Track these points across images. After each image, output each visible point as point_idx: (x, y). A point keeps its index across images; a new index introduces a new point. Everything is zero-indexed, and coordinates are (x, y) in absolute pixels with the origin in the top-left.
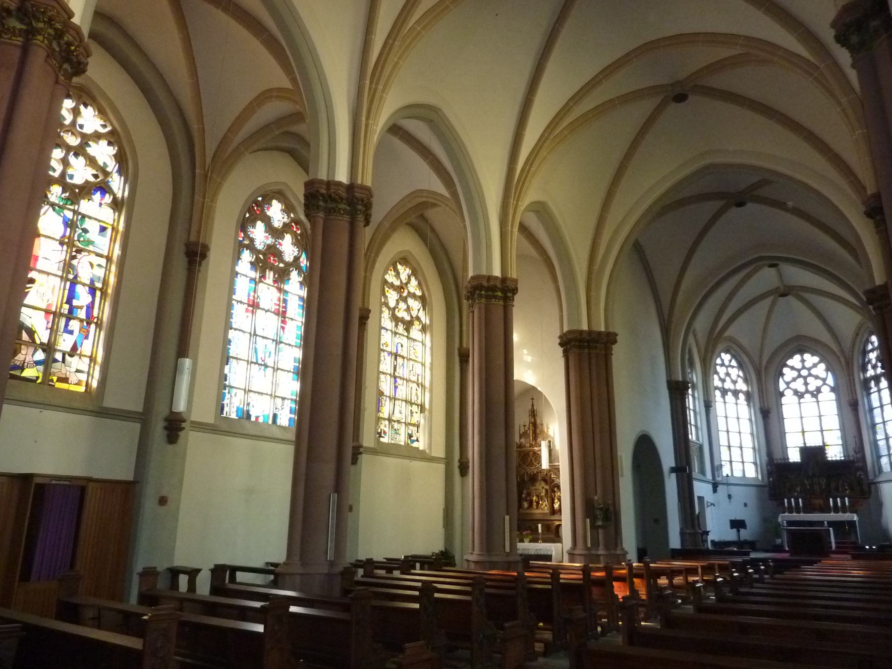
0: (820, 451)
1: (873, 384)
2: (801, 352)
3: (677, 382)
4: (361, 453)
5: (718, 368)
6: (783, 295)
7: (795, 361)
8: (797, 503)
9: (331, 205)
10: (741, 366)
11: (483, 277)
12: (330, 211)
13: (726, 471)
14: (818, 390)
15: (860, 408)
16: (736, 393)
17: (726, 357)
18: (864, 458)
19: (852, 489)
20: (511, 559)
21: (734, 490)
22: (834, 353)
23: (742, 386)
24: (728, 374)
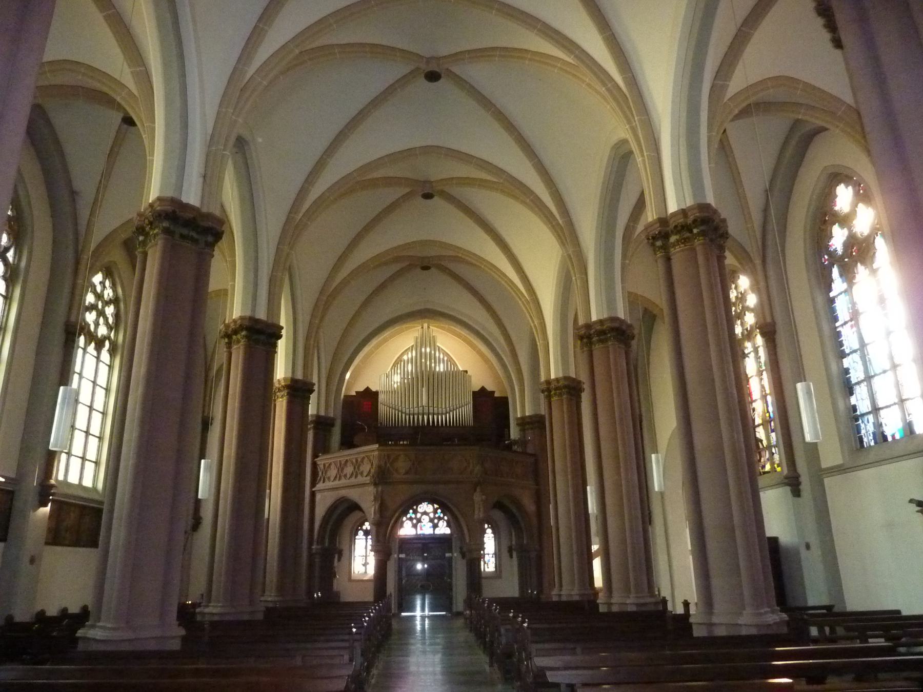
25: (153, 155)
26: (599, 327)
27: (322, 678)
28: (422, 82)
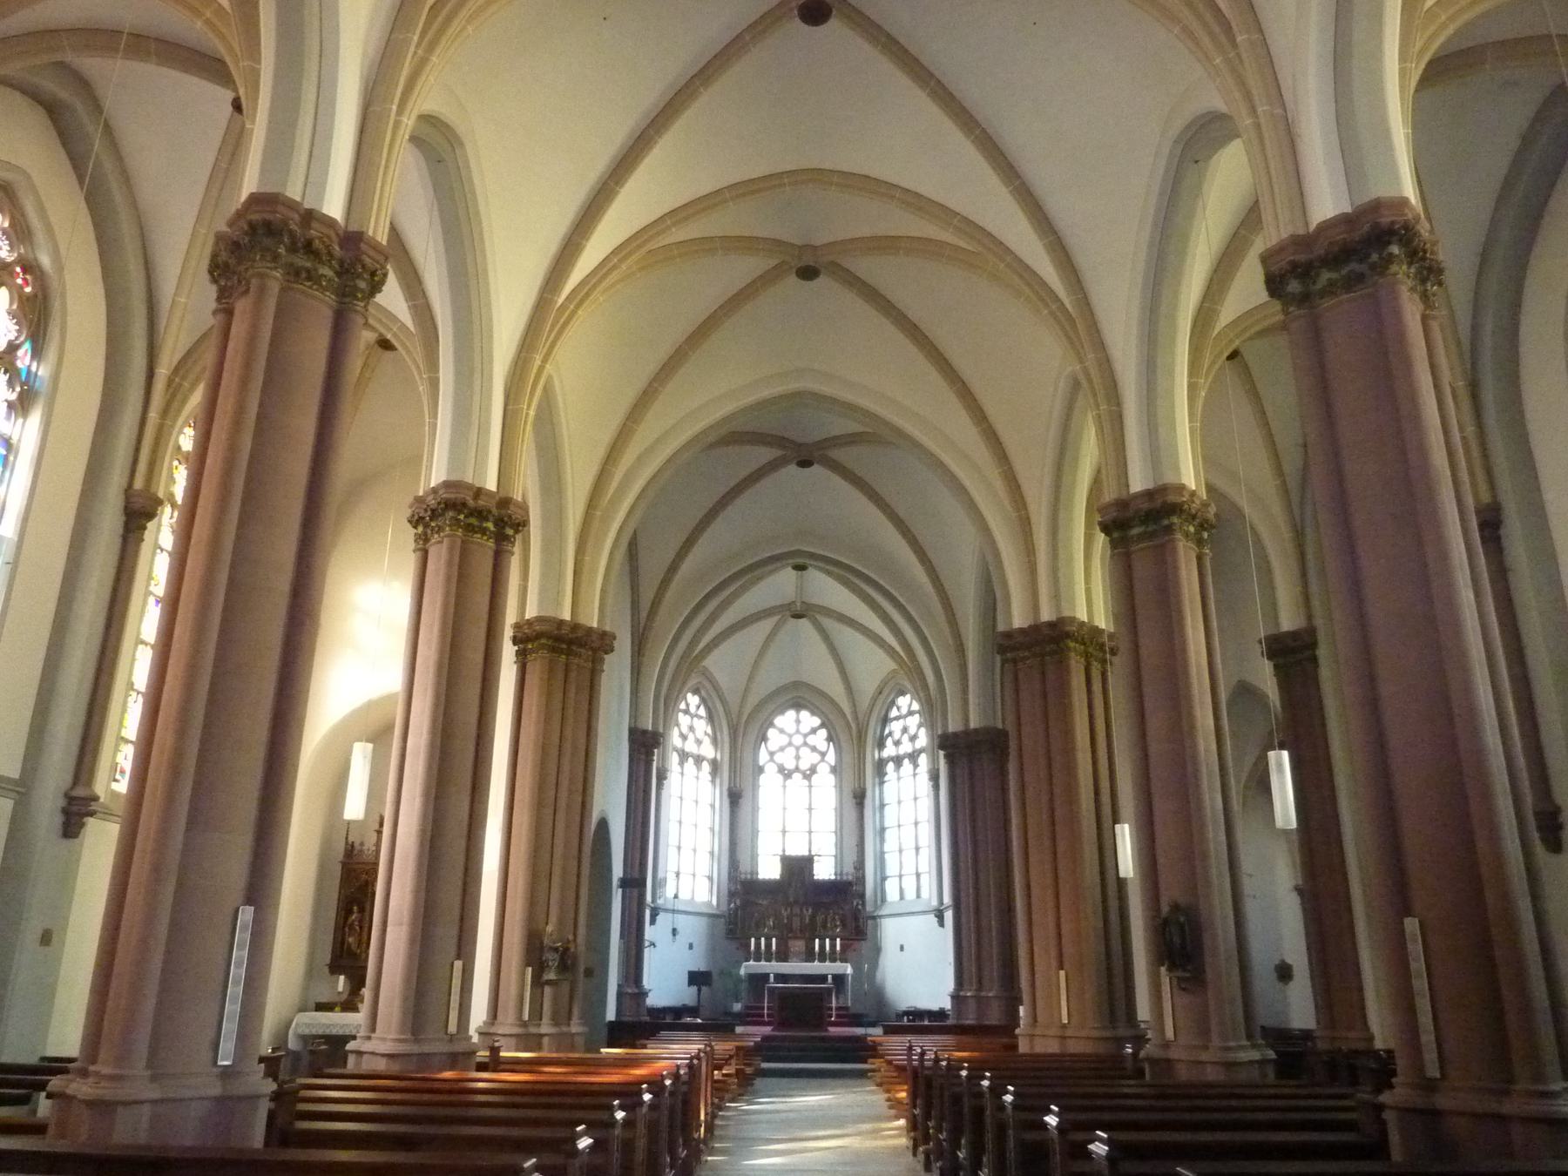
0: (806, 863)
1: (890, 767)
2: (798, 706)
3: (645, 732)
4: (92, 814)
5: (681, 715)
6: (798, 616)
7: (786, 720)
8: (768, 945)
9: (302, 261)
10: (711, 718)
11: (469, 487)
12: (297, 274)
13: (670, 891)
14: (813, 770)
15: (868, 802)
16: (699, 760)
17: (693, 700)
18: (861, 880)
19: (844, 925)
20: (459, 1047)
21: (682, 922)
22: (844, 715)
23: (708, 751)
24: (691, 728)
25: (253, 122)
26: (1146, 506)
27: (972, 775)
28: (793, 279)
